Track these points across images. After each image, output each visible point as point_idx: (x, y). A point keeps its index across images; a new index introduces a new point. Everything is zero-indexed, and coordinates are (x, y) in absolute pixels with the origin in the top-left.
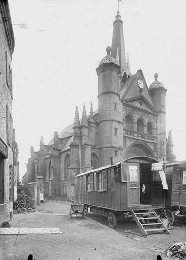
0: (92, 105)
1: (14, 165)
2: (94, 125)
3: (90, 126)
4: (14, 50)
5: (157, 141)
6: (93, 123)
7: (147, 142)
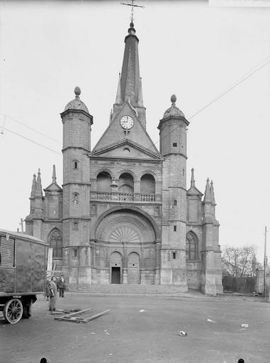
0: (54, 168)
1: (123, 267)
2: (56, 193)
3: (51, 195)
4: (141, 75)
5: (161, 201)
6: (56, 191)
7: (139, 204)
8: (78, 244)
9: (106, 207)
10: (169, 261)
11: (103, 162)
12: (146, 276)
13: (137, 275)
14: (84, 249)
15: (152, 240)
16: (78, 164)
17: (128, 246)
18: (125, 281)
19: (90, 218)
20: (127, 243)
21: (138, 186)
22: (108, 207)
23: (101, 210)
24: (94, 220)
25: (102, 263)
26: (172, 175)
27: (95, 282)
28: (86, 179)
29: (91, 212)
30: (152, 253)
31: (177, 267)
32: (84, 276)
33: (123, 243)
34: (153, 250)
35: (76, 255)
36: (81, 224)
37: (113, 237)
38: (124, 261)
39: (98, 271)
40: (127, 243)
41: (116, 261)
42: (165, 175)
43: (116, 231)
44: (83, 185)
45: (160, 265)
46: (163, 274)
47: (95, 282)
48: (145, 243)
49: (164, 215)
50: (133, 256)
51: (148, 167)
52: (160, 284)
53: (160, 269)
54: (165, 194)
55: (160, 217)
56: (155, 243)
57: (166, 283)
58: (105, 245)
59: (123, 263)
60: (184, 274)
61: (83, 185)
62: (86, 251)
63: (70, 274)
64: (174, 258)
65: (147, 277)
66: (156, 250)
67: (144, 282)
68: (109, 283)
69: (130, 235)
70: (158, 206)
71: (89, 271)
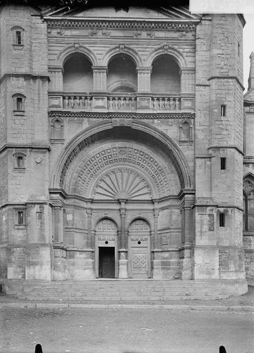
1: (120, 246)
8: (24, 201)
9: (81, 123)
10: (211, 229)
11: (75, 32)
12: (163, 263)
13: (147, 261)
14: (37, 208)
15: (175, 191)
16: (24, 36)
17: (129, 206)
18: (123, 272)
19: (48, 144)
20: (127, 201)
21: (144, 82)
22: (86, 124)
23: (72, 131)
24: (58, 151)
25: (79, 240)
26: (215, 51)
27: (60, 275)
28: (40, 68)
29: (51, 134)
30: (174, 217)
31: (227, 244)
32: (34, 264)
33: (119, 202)
34: (178, 211)
35: (21, 222)
36: (31, 159)
37: (99, 190)
38: (122, 235)
39: (70, 253)
40: (127, 201)
41: (107, 236)
42: (201, 54)
43: (107, 179)
44: (35, 78)
45: (193, 240)
46: (199, 257)
47: (60, 275)
48: (161, 200)
49: (200, 136)
50: (137, 227)
51: (166, 39)
52: (192, 279)
53: (192, 248)
54: (202, 96)
55: (191, 141)
56: (181, 196)
57: (207, 277)
58: (84, 205)
59: (120, 239)
60: (240, 258)
61: (35, 78)
62: (41, 213)
63: (9, 261)
64: (222, 224)
65: (165, 265)
66: (183, 210)
67: (158, 275)
68: (93, 278)
69: (133, 176)
70: (187, 120)
71: (46, 253)
